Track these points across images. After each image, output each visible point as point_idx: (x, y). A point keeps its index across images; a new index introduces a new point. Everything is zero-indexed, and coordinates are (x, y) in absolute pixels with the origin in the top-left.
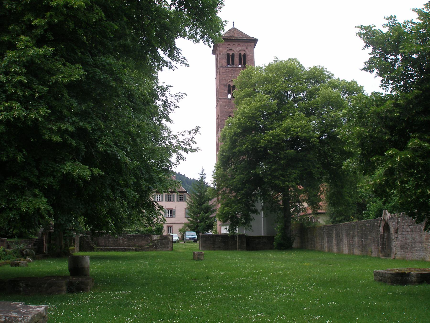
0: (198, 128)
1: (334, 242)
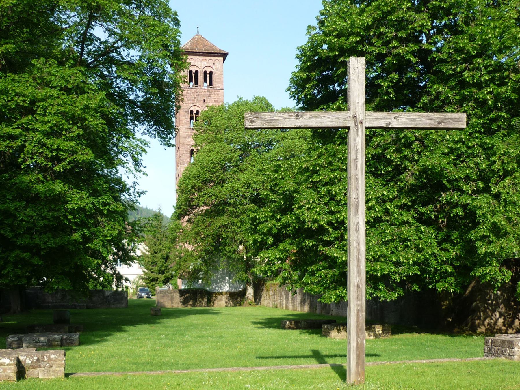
0: (146, 191)
1: (290, 299)
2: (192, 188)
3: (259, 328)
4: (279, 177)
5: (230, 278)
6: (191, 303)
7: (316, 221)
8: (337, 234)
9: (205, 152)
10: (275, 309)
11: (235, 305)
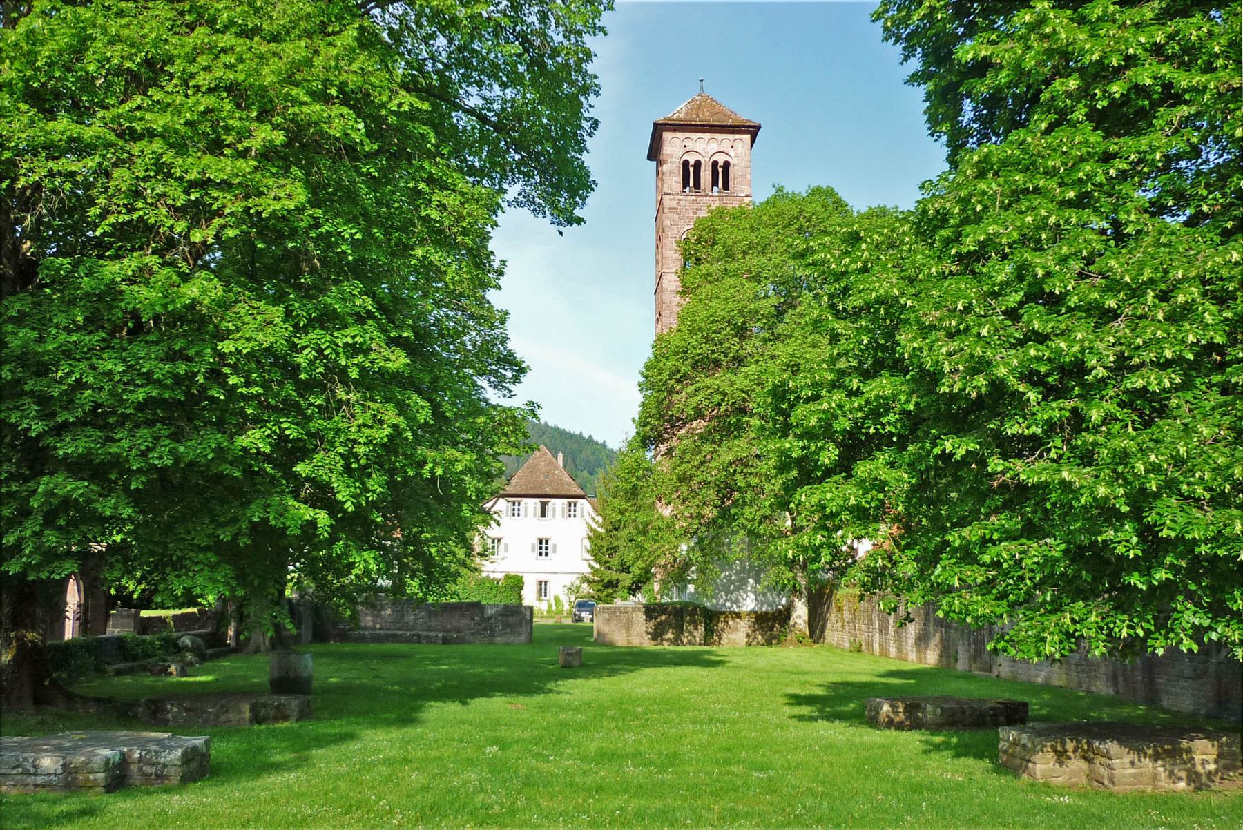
1: (891, 631)
2: (671, 376)
3: (801, 718)
4: (853, 266)
5: (757, 581)
6: (670, 635)
7: (980, 366)
8: (1057, 410)
9: (701, 300)
10: (856, 654)
11: (769, 643)
